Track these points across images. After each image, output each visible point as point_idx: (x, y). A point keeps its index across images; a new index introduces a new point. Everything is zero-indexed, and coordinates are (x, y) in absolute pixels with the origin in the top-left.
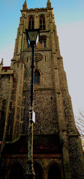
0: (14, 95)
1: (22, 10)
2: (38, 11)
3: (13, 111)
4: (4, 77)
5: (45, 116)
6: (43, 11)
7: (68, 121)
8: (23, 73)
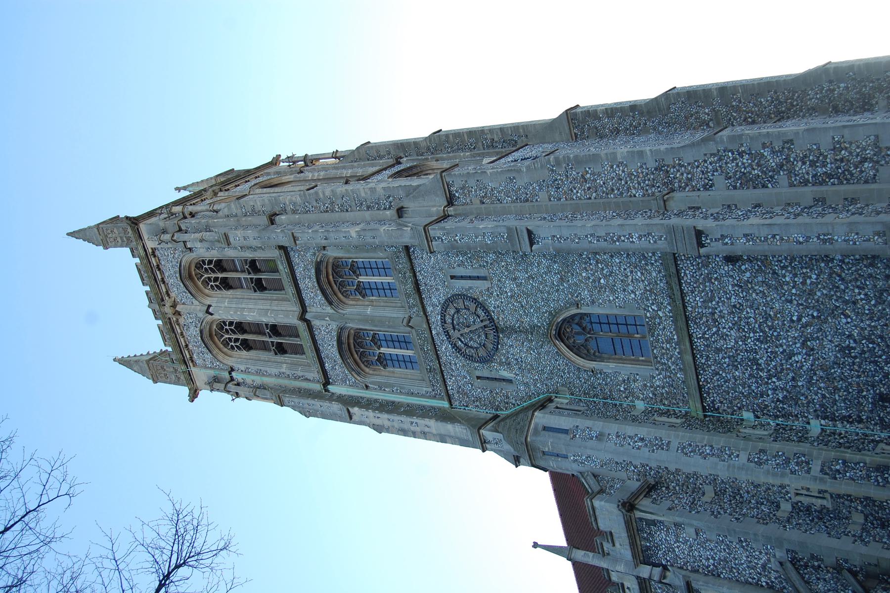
0: (748, 492)
1: (185, 391)
2: (168, 302)
3: (851, 501)
4: (648, 548)
5: (855, 303)
6: (162, 273)
7: (878, 162)
8: (598, 425)
